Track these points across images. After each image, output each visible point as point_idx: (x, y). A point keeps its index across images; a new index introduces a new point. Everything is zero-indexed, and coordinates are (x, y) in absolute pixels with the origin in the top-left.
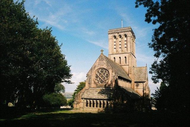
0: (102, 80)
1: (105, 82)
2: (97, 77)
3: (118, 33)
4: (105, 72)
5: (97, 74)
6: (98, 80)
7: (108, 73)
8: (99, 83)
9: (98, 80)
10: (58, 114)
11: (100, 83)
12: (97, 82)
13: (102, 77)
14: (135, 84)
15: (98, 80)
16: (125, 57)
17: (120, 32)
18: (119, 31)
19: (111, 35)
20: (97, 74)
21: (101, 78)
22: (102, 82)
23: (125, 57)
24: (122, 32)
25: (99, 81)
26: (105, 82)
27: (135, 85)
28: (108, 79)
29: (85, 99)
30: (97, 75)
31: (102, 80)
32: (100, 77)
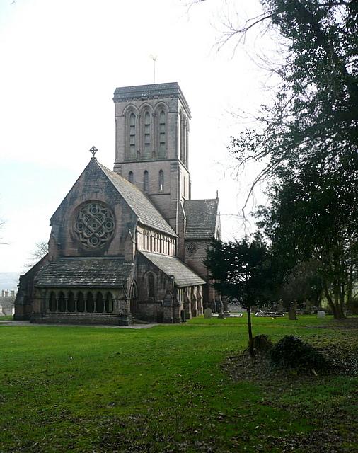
6: (83, 236)
15: (83, 236)
21: (92, 229)
32: (89, 226)
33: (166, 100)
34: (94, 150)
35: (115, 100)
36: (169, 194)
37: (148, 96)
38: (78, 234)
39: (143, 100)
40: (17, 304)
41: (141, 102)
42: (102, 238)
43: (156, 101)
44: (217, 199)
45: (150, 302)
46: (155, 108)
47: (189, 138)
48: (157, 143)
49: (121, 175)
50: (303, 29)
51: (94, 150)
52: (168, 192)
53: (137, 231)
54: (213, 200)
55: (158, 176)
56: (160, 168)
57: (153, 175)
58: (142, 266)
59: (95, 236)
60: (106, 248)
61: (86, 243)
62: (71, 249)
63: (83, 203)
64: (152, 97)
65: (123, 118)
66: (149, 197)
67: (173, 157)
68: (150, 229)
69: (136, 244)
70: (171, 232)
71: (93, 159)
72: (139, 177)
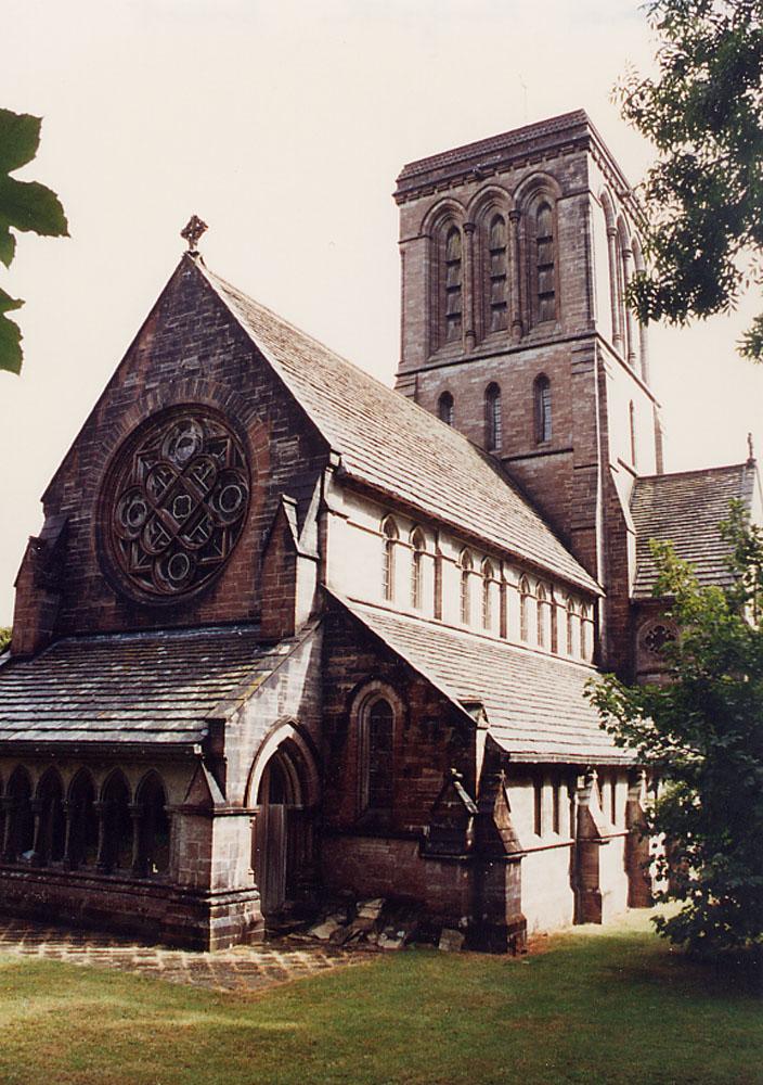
33: (551, 165)
34: (194, 230)
35: (401, 197)
36: (571, 450)
37: (495, 166)
39: (480, 178)
40: (224, 727)
41: (473, 188)
42: (202, 552)
43: (520, 173)
44: (751, 464)
45: (373, 830)
46: (516, 196)
47: (626, 176)
48: (529, 295)
49: (416, 397)
50: (736, 598)
51: (194, 230)
52: (566, 443)
53: (324, 508)
54: (738, 468)
55: (531, 396)
56: (539, 369)
57: (516, 396)
58: (344, 661)
59: (182, 549)
60: (210, 594)
63: (146, 423)
64: (507, 165)
65: (422, 243)
66: (503, 467)
67: (583, 328)
68: (427, 525)
69: (321, 563)
70: (564, 564)
71: (188, 261)
72: (471, 408)
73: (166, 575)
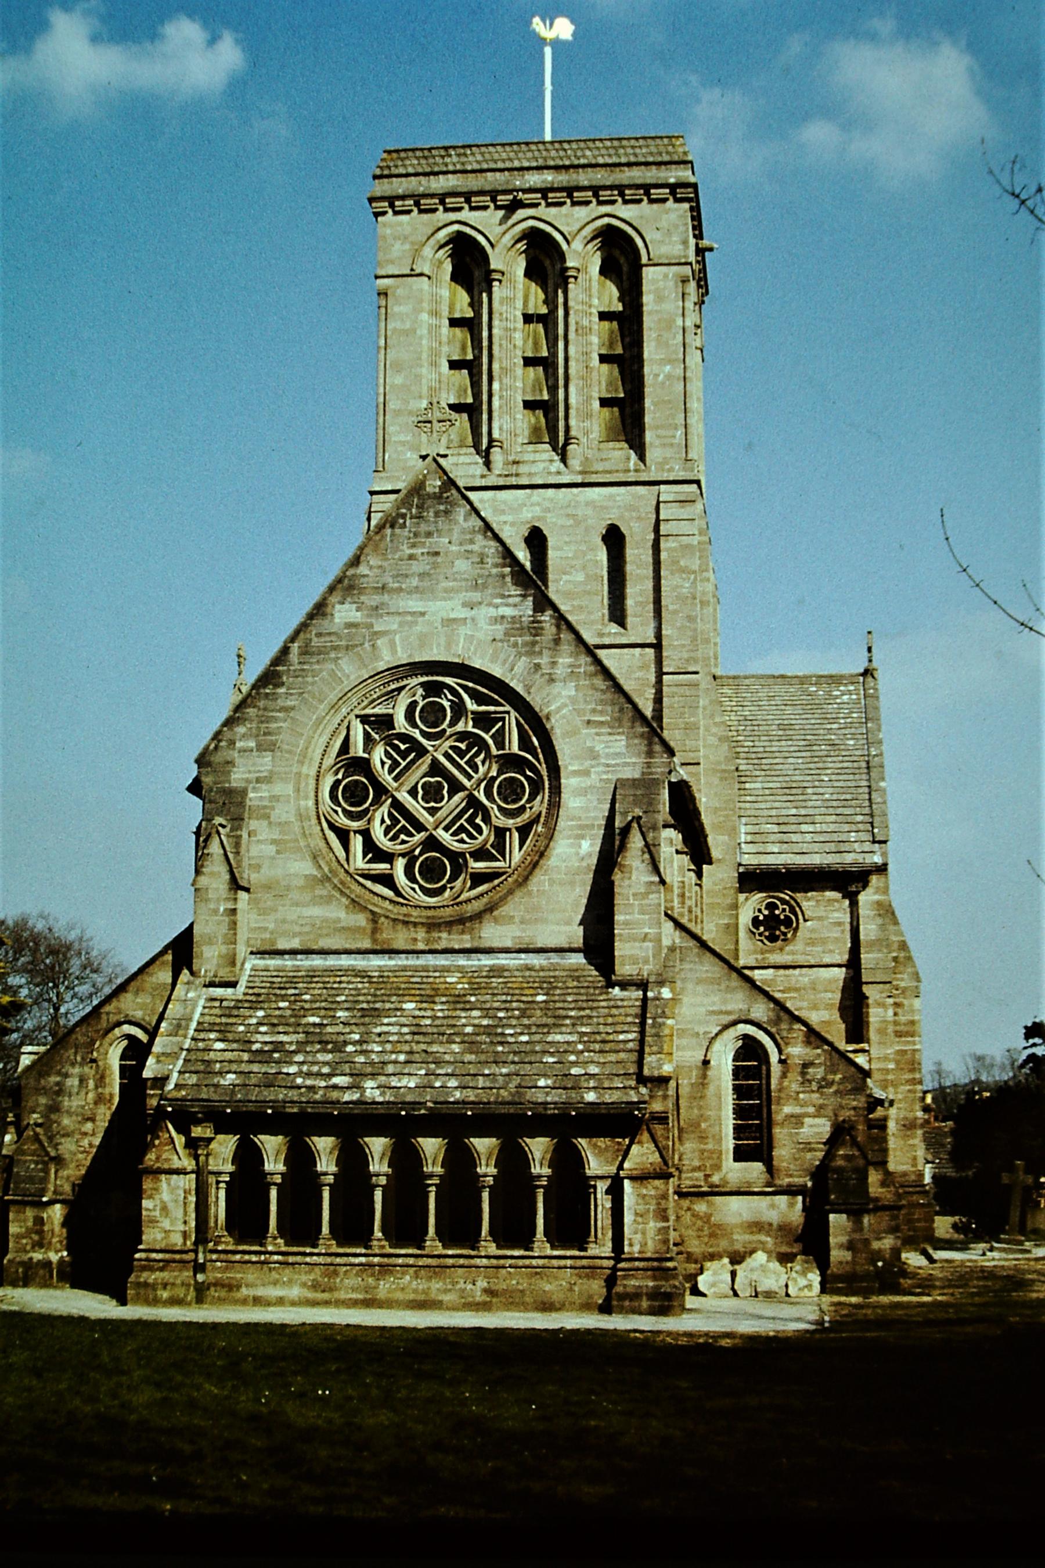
0: (432, 843)
1: (479, 866)
2: (354, 794)
3: (515, 205)
4: (483, 721)
5: (358, 749)
6: (370, 845)
7: (525, 743)
8: (387, 880)
9: (378, 832)
10: (1032, 1301)
11: (401, 878)
12: (359, 861)
13: (432, 794)
14: (752, 905)
15: (370, 845)
16: (614, 538)
17: (544, 192)
18: (534, 179)
19: (414, 223)
20: (358, 749)
21: (416, 807)
22: (432, 871)
23: (614, 538)
24: (570, 191)
25: (388, 857)
26: (479, 866)
27: (745, 917)
28: (524, 832)
29: (223, 1124)
30: (362, 765)
31: (445, 837)
32: (403, 797)
38: (343, 835)
61: (387, 880)
62: (316, 911)
73: (411, 877)
